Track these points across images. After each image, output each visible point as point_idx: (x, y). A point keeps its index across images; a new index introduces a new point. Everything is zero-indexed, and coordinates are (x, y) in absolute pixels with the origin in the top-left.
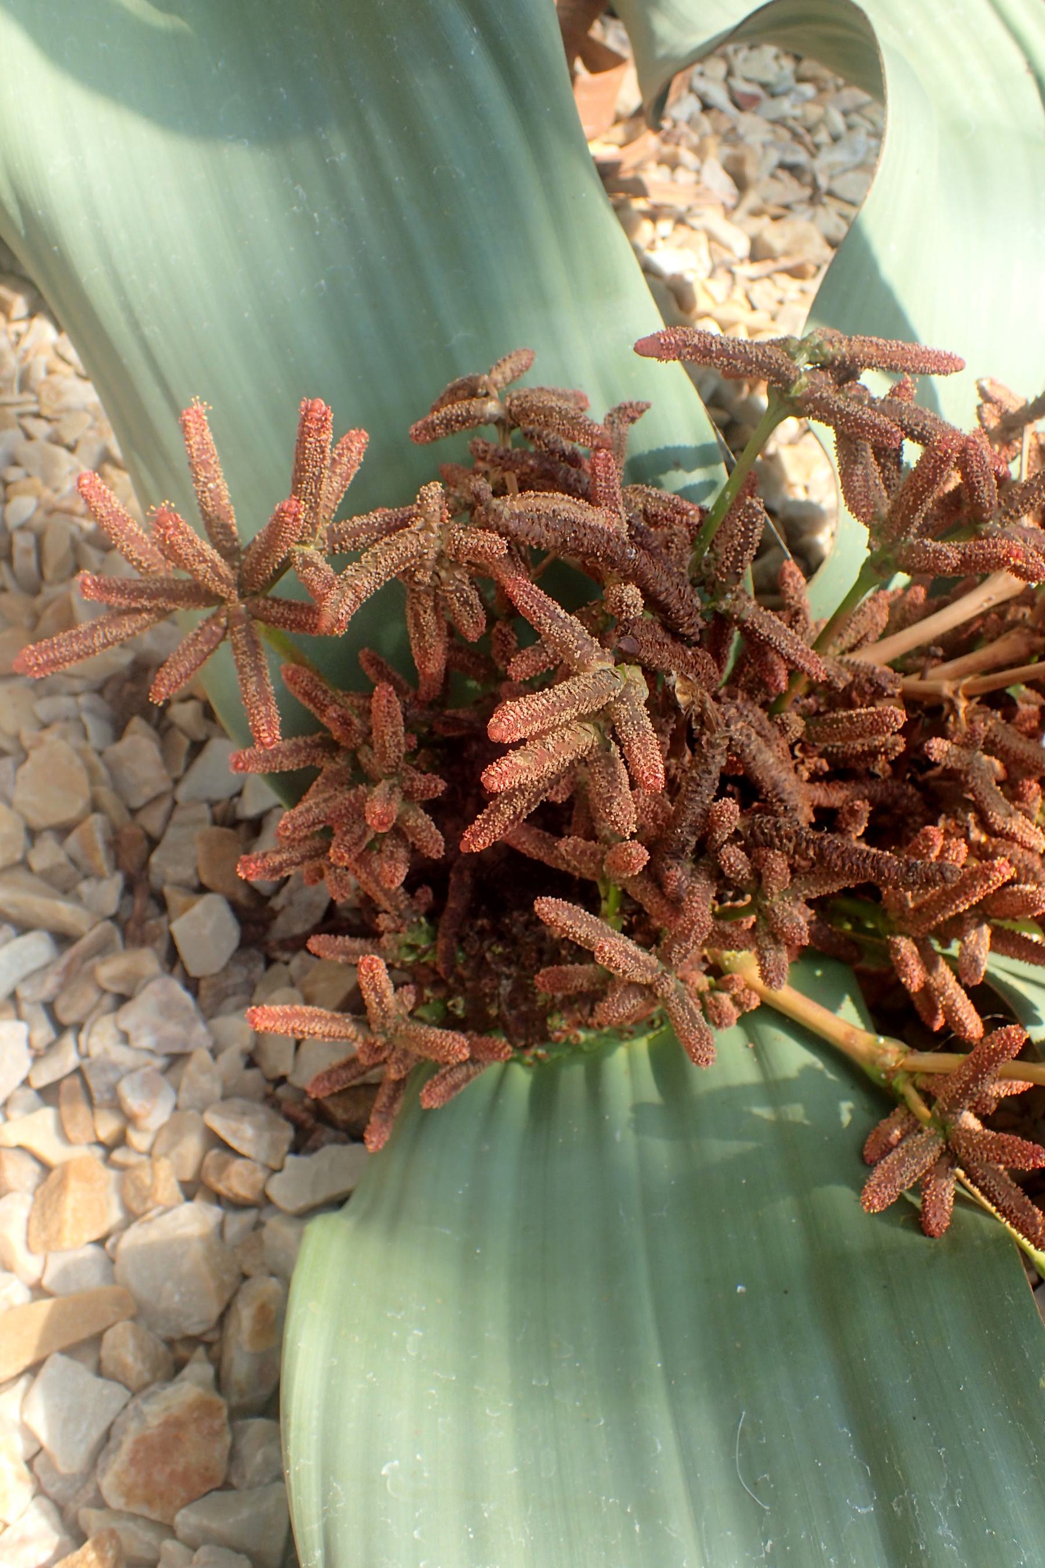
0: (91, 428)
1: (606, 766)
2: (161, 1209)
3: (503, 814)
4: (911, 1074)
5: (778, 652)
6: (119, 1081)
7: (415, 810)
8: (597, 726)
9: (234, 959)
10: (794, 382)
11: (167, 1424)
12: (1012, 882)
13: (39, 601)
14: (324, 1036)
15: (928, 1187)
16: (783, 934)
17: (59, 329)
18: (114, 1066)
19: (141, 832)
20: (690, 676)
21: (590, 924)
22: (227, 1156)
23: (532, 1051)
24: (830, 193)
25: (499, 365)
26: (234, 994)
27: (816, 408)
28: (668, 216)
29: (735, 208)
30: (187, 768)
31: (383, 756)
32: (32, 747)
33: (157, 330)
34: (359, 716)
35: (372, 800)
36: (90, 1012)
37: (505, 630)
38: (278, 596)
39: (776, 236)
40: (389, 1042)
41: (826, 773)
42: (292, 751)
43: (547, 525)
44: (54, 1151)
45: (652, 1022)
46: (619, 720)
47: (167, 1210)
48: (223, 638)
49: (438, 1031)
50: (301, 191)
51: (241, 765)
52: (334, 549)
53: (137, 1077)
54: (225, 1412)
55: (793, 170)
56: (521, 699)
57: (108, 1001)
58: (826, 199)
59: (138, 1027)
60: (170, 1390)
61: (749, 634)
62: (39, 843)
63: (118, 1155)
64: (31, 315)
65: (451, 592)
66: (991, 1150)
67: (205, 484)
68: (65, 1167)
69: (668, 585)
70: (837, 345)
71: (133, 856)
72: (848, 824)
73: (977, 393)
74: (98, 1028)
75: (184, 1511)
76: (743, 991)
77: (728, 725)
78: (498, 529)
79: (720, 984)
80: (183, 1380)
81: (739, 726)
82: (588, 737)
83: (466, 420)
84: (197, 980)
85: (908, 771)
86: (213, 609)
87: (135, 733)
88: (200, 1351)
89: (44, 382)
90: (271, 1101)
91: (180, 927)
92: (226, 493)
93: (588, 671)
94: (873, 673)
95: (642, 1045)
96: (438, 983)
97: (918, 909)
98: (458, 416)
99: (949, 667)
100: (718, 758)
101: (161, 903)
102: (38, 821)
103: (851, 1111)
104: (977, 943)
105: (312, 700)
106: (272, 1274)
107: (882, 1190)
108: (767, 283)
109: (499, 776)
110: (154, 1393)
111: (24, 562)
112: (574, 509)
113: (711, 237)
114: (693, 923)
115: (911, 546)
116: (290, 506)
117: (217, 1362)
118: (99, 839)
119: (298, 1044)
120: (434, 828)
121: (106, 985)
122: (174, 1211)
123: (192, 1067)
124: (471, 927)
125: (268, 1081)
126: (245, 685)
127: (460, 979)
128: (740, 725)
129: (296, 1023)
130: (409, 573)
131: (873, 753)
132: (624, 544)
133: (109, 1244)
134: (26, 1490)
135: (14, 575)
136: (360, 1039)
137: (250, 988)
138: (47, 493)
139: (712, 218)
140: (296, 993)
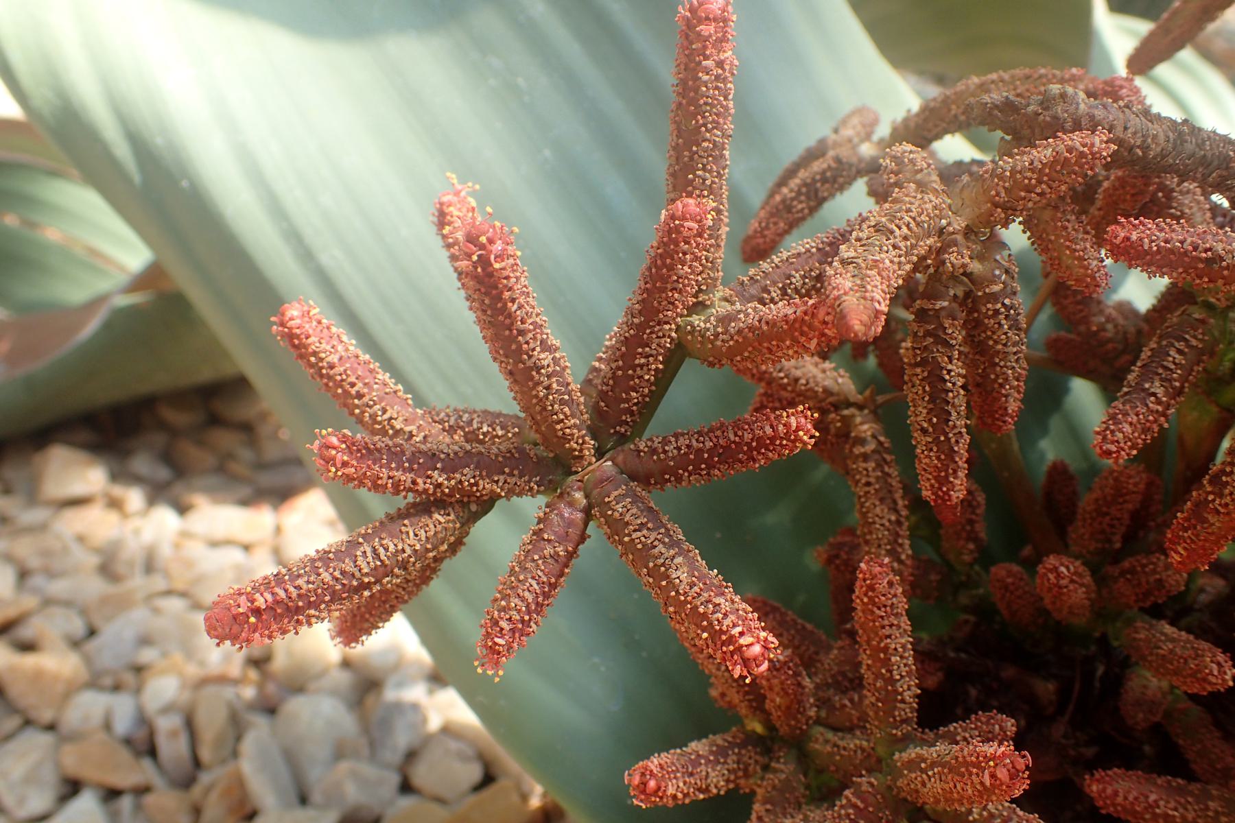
13: (197, 790)
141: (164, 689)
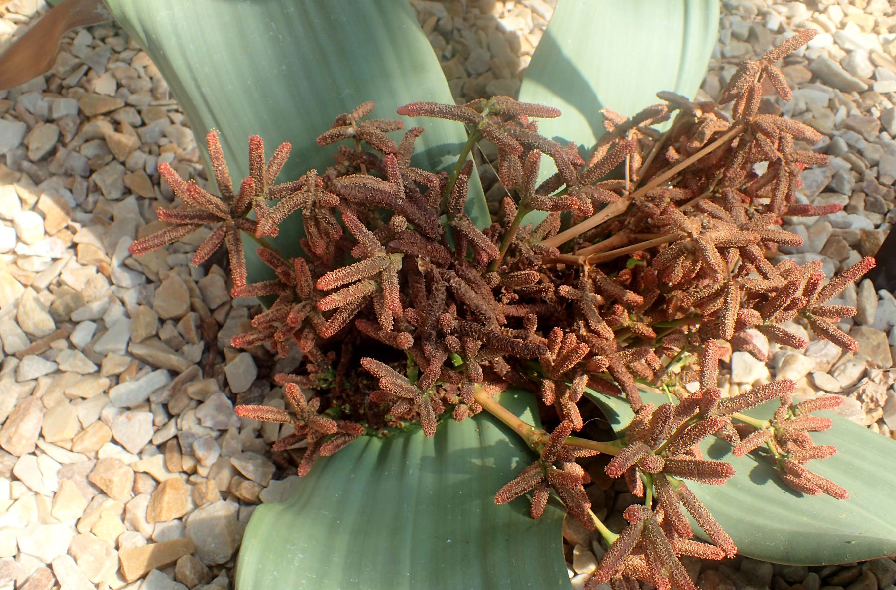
18: (193, 435)
19: (214, 322)
22: (242, 479)
32: (164, 279)
36: (185, 408)
42: (262, 287)
44: (162, 475)
57: (193, 404)
59: (205, 416)
62: (165, 326)
63: (192, 478)
68: (165, 482)
71: (209, 332)
74: (186, 417)
84: (236, 394)
86: (221, 223)
87: (213, 272)
88: (224, 571)
91: (229, 369)
92: (227, 170)
100: (440, 295)
102: (165, 315)
103: (517, 462)
105: (272, 263)
113: (534, 11)
121: (192, 397)
127: (348, 396)
129: (259, 414)
130: (300, 210)
135: (161, 191)
138: (180, 151)
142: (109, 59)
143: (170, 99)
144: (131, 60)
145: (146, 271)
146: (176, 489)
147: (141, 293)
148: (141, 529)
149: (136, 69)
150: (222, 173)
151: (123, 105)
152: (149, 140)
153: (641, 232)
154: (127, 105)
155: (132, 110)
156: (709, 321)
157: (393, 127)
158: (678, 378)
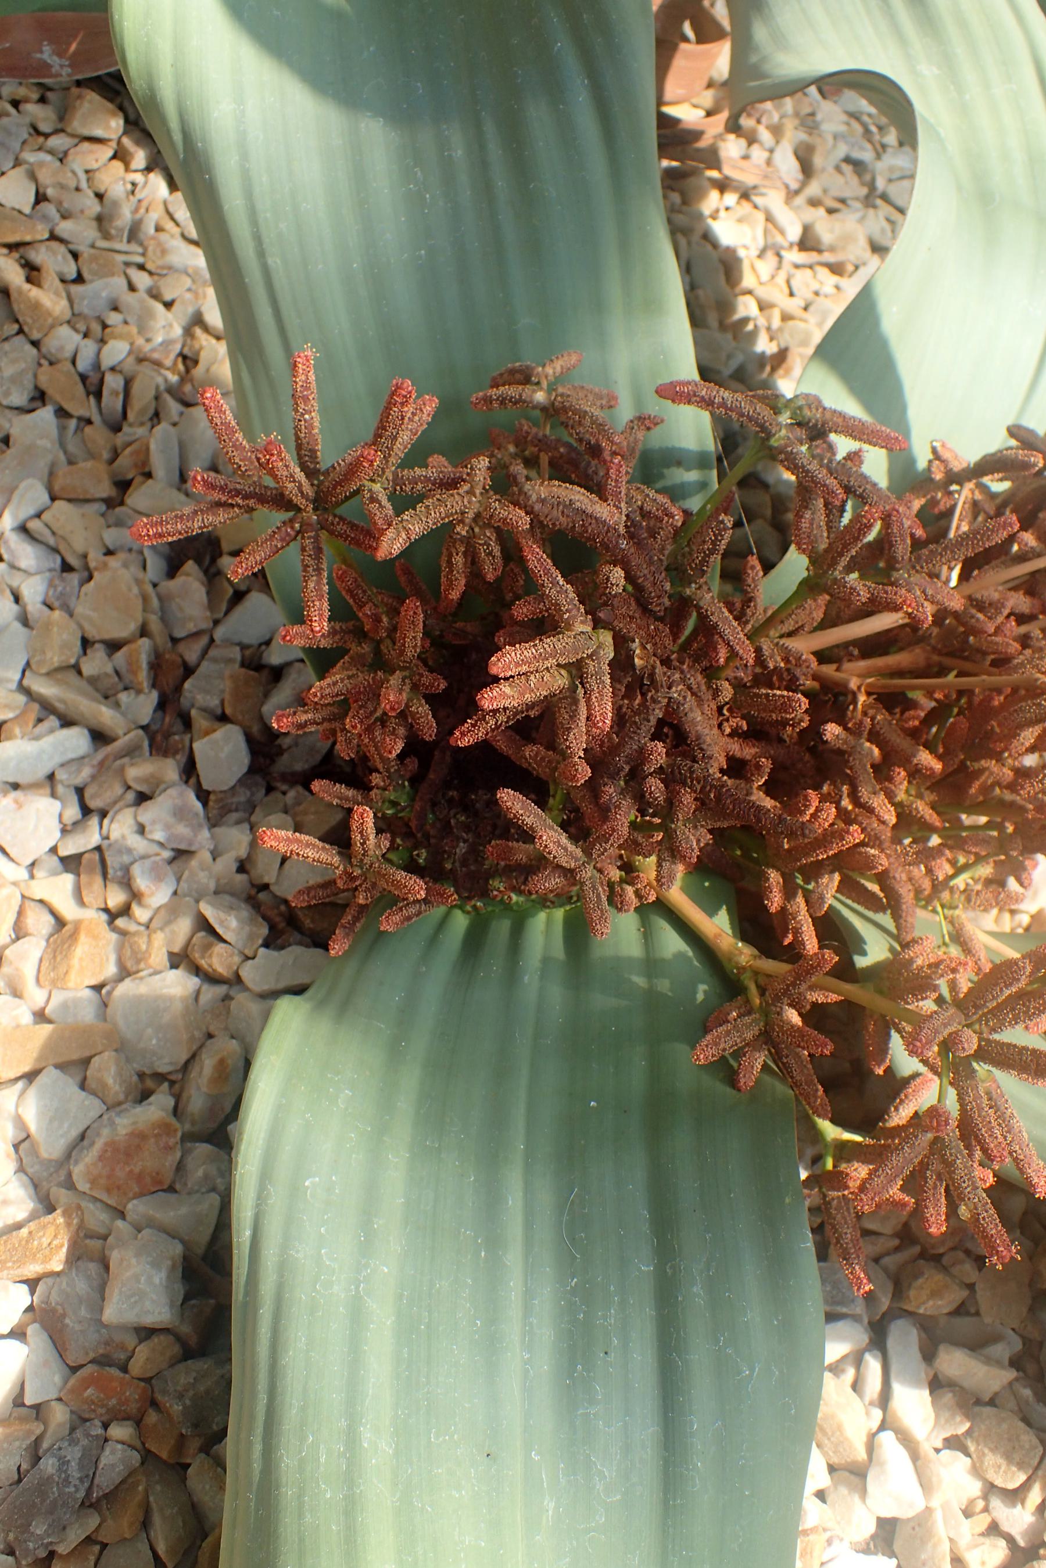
0: (189, 290)
1: (571, 704)
2: (151, 971)
3: (487, 723)
4: (756, 973)
5: (721, 636)
6: (132, 863)
7: (418, 699)
8: (569, 672)
9: (241, 781)
10: (774, 435)
11: (132, 1134)
12: (862, 844)
13: (120, 439)
14: (314, 860)
15: (745, 1056)
16: (679, 852)
17: (173, 186)
18: (129, 851)
20: (648, 646)
21: (536, 815)
22: (211, 939)
23: (473, 902)
24: (884, 197)
25: (552, 361)
26: (237, 810)
27: (786, 459)
28: (735, 189)
29: (797, 192)
30: (227, 613)
31: (402, 652)
32: (96, 569)
33: (279, 262)
34: (388, 614)
35: (387, 688)
36: (115, 803)
37: (516, 570)
38: (345, 516)
39: (826, 230)
40: (364, 874)
41: (744, 732)
43: (563, 512)
44: (69, 910)
45: (571, 897)
46: (587, 673)
47: (156, 973)
48: (295, 539)
49: (404, 874)
50: (419, 174)
51: (288, 638)
52: (396, 490)
53: (148, 863)
54: (179, 1134)
55: (858, 166)
56: (517, 646)
57: (130, 796)
58: (879, 202)
59: (154, 822)
60: (139, 1110)
61: (703, 618)
63: (120, 922)
64: (148, 169)
65: (480, 544)
66: (794, 1037)
67: (303, 415)
68: (78, 924)
69: (646, 572)
70: (814, 410)
71: (170, 676)
72: (753, 775)
73: (930, 450)
74: (119, 817)
75: (135, 1202)
76: (645, 887)
77: (670, 688)
78: (525, 507)
79: (629, 879)
80: (150, 1104)
81: (679, 688)
82: (561, 681)
83: (518, 401)
84: (208, 793)
85: (813, 740)
86: (291, 514)
87: (188, 575)
88: (166, 1085)
89: (153, 238)
90: (252, 901)
92: (317, 424)
93: (571, 631)
94: (800, 658)
95: (559, 914)
96: (409, 834)
97: (789, 851)
98: (512, 397)
99: (863, 664)
100: (657, 711)
101: (187, 723)
102: (92, 633)
103: (705, 992)
104: (827, 886)
105: (353, 596)
106: (233, 1037)
107: (707, 1052)
108: (808, 271)
109: (491, 699)
110: (126, 1110)
111: (112, 402)
112: (586, 501)
113: (769, 218)
114: (614, 830)
115: (836, 579)
116: (369, 454)
117: (178, 1098)
118: (144, 660)
119: (284, 860)
120: (430, 717)
121: (131, 784)
122: (163, 974)
123: (194, 863)
124: (444, 795)
125: (253, 885)
126: (306, 582)
127: (427, 836)
128: (681, 687)
130: (451, 525)
131: (784, 723)
132: (619, 536)
133: (104, 991)
134: (11, 1166)
136: (341, 867)
137: (251, 807)
138: (140, 341)
139: (773, 200)
140: (289, 819)
141: (116, 351)
142: (24, 142)
143: (129, 241)
144: (66, 153)
145: (62, 548)
146: (95, 937)
147: (51, 584)
148: (25, 995)
149: (74, 172)
150: (310, 427)
151: (46, 235)
152: (86, 311)
153: (951, 654)
154: (53, 237)
155: (62, 249)
156: (1034, 820)
157: (604, 402)
158: (963, 898)
